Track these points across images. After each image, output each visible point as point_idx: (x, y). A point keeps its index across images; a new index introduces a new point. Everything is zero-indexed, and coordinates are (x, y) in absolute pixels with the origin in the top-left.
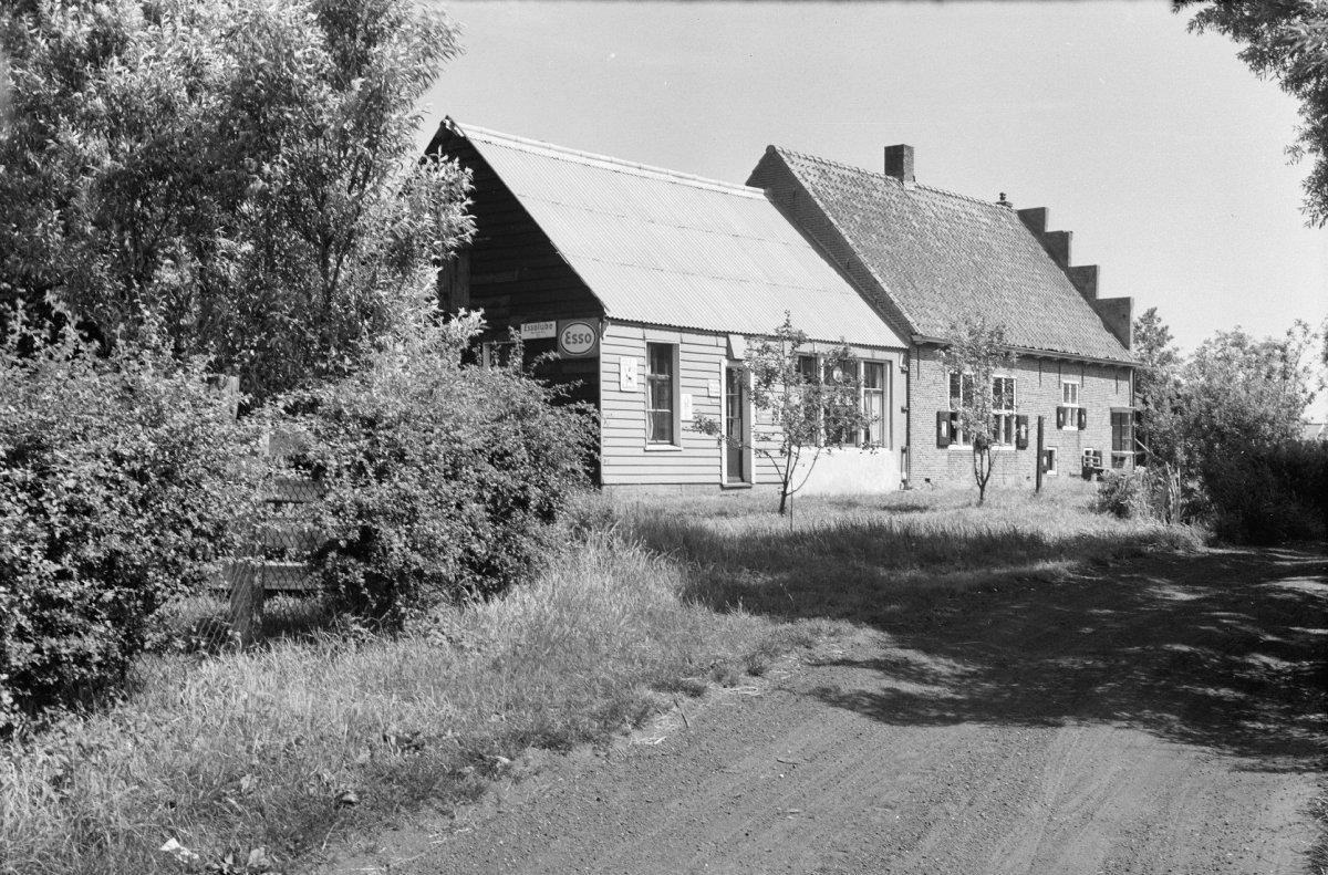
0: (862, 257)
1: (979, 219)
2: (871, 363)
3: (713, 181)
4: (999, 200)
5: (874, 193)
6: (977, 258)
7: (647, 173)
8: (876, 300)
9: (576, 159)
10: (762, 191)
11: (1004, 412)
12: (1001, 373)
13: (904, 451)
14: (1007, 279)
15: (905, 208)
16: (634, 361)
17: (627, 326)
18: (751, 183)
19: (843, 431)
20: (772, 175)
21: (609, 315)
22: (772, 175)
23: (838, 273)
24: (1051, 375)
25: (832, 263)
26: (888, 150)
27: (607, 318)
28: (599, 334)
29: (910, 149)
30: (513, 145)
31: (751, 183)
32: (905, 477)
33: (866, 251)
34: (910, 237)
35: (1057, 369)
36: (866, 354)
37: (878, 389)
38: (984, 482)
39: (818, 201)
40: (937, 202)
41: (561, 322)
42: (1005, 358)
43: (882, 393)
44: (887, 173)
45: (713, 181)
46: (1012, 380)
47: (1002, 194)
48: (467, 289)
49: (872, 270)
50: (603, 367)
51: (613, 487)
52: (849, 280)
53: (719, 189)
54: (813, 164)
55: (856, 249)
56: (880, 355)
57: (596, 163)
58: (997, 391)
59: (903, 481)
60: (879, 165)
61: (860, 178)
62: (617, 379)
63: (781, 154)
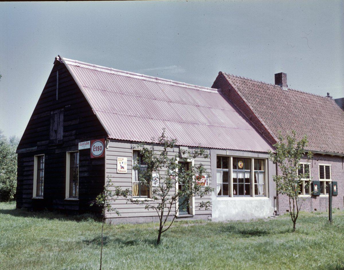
0: (257, 115)
1: (317, 102)
2: (258, 159)
3: (193, 85)
4: (327, 95)
5: (268, 91)
6: (315, 116)
7: (160, 81)
8: (263, 132)
9: (123, 74)
10: (217, 89)
11: (325, 180)
12: (303, 162)
13: (275, 198)
14: (328, 125)
15: (282, 97)
16: (125, 159)
17: (122, 142)
18: (213, 87)
19: (244, 188)
20: (221, 84)
21: (110, 137)
22: (221, 84)
23: (247, 121)
24: (339, 163)
25: (244, 117)
26: (276, 75)
27: (109, 139)
28: (105, 146)
29: (285, 75)
30: (92, 68)
31: (213, 87)
32: (276, 209)
33: (260, 112)
34: (283, 107)
35: (341, 161)
36: (256, 155)
37: (262, 171)
38: (296, 219)
39: (239, 93)
40: (297, 95)
41: (92, 141)
42: (306, 155)
43: (264, 173)
44: (276, 84)
45: (193, 85)
46: (308, 166)
47: (328, 93)
48: (62, 128)
49: (261, 120)
50: (106, 162)
51: (112, 219)
52: (251, 124)
53: (195, 88)
54: (240, 79)
55: (254, 111)
56: (261, 156)
57: (135, 77)
58: (300, 171)
59: (275, 212)
60: (272, 81)
61: (262, 86)
62: (210, 164)
63: (225, 75)
